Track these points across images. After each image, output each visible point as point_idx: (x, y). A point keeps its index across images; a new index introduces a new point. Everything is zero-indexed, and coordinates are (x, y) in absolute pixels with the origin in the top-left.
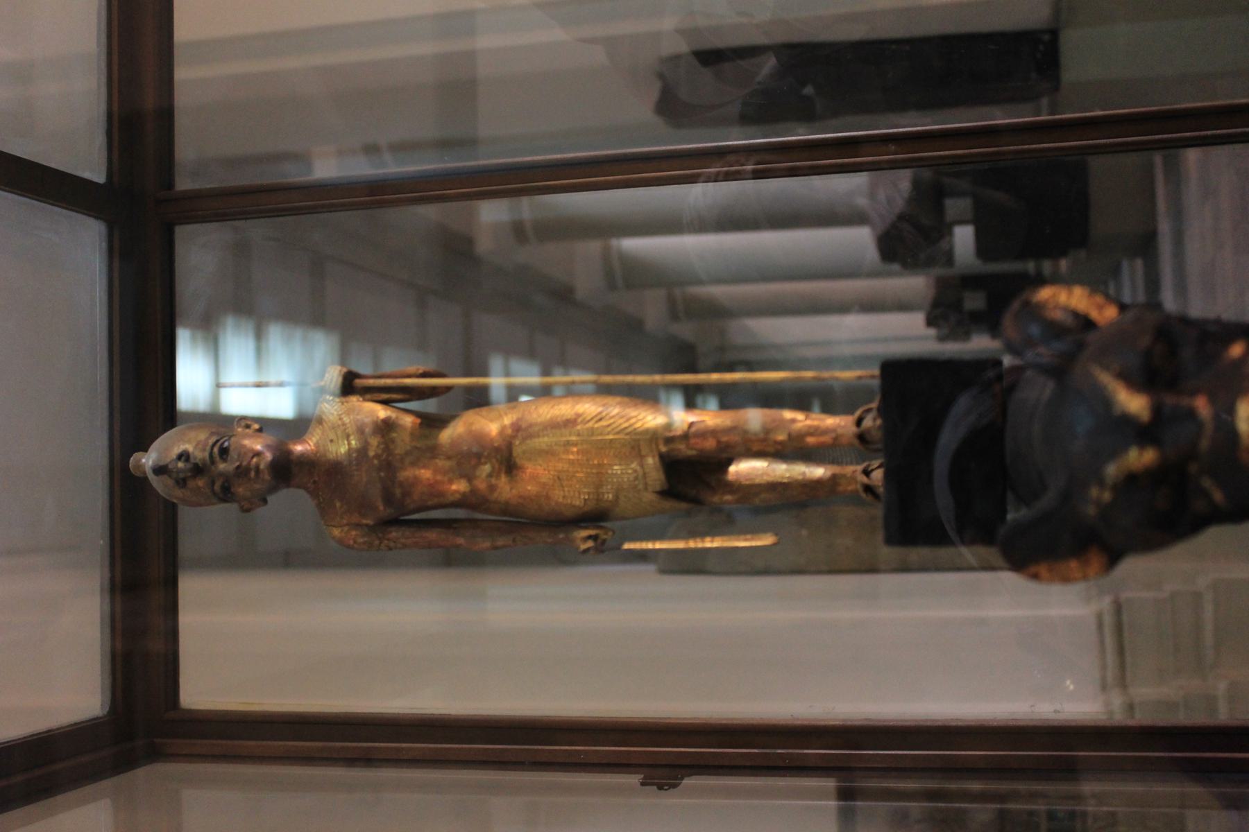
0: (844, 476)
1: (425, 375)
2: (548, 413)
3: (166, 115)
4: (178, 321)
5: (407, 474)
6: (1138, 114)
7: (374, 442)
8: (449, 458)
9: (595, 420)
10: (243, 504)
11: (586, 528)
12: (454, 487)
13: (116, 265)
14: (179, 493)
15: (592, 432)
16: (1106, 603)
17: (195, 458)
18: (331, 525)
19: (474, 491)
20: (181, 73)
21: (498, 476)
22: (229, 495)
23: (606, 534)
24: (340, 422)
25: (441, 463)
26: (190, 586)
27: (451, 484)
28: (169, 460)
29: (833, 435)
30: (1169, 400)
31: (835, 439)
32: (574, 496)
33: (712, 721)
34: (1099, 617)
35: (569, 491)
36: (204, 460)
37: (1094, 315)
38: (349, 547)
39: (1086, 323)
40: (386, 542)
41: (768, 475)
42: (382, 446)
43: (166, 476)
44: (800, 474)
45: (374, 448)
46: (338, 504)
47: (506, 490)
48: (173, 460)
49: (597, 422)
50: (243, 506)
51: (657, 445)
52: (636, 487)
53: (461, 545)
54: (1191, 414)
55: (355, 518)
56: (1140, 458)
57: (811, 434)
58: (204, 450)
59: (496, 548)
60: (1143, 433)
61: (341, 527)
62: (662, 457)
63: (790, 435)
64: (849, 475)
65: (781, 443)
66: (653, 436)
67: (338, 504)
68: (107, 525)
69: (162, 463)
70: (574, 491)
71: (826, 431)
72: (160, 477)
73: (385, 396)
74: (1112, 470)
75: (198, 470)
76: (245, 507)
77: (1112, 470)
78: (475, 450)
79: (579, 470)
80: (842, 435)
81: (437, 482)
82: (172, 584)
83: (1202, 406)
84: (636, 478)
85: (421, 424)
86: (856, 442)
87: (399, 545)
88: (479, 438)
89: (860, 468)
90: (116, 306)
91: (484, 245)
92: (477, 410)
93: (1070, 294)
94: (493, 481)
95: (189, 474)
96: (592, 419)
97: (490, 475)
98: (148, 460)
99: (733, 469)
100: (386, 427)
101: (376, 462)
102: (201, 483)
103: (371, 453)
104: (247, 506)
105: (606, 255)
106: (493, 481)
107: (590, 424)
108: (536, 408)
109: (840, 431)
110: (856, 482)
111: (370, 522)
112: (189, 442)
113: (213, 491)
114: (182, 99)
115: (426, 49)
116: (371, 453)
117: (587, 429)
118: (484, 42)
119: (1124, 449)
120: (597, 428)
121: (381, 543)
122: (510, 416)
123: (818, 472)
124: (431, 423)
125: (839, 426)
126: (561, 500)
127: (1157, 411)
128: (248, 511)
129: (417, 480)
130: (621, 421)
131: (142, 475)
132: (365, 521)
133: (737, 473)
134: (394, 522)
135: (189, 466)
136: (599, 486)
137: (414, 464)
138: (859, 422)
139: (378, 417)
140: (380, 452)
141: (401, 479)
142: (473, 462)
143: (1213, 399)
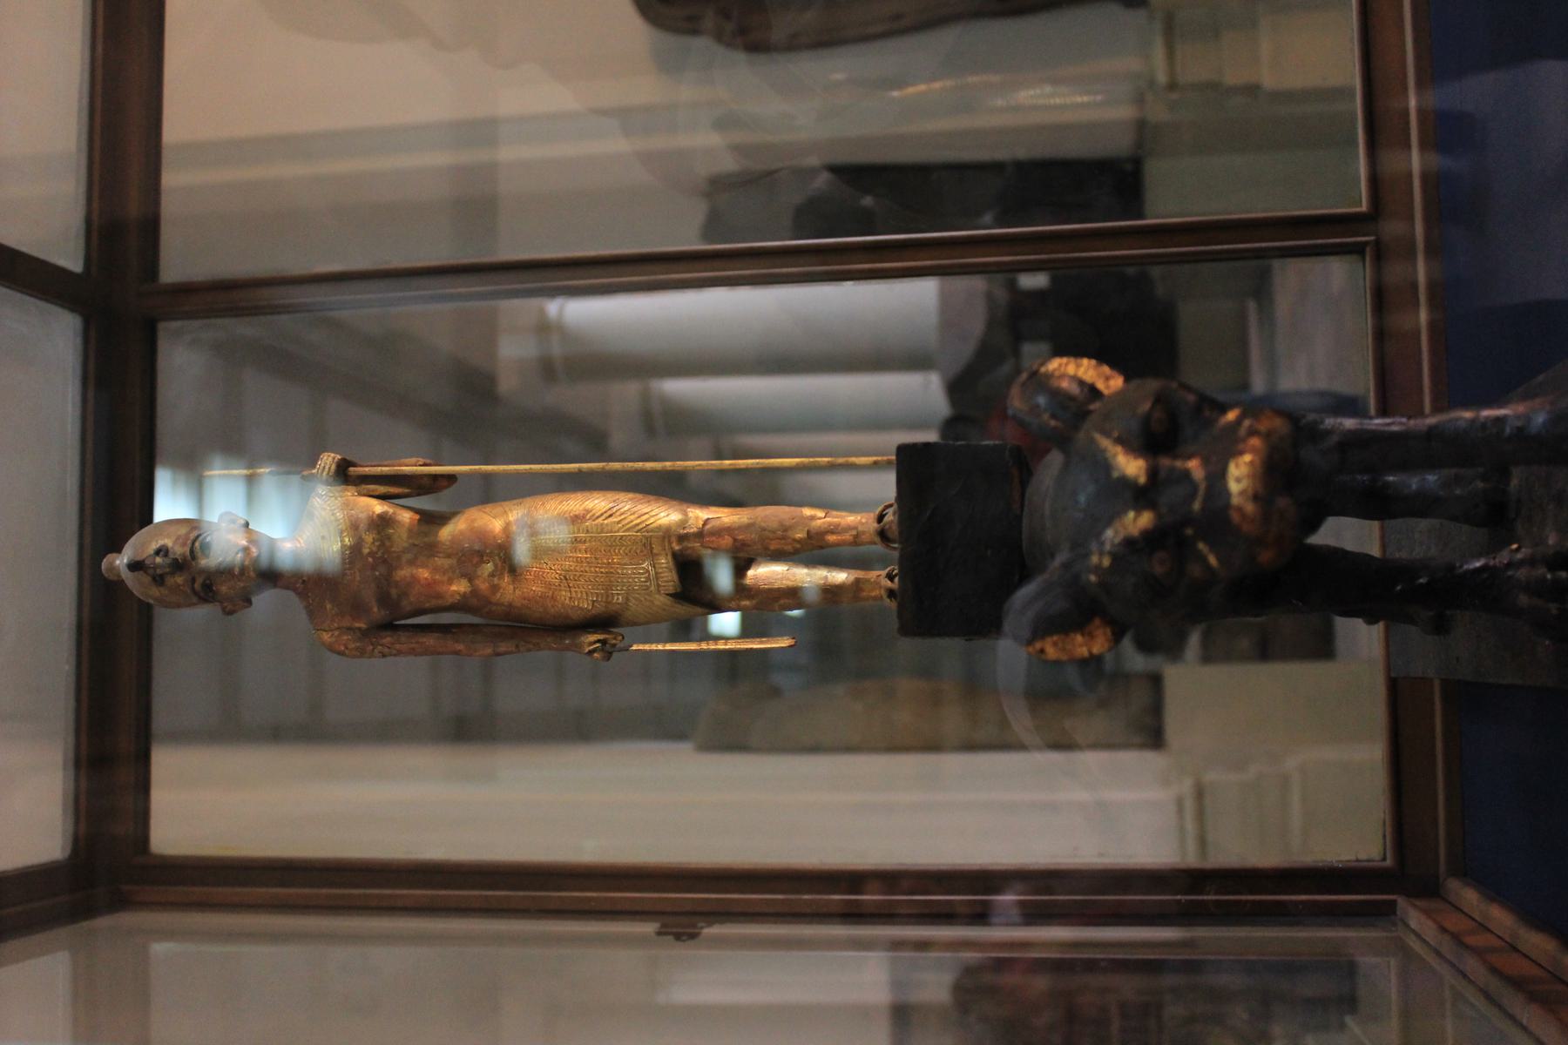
0: (868, 581)
1: (425, 465)
2: (555, 509)
3: (151, 226)
4: (158, 459)
5: (403, 573)
6: (1192, 223)
7: (369, 538)
8: (449, 556)
9: (603, 517)
10: (225, 604)
11: (595, 633)
12: (454, 588)
13: (91, 394)
14: (155, 591)
15: (602, 528)
16: (1187, 786)
17: (175, 554)
18: (321, 630)
19: (475, 592)
20: (171, 178)
21: (501, 576)
22: (210, 594)
23: (615, 639)
24: (333, 518)
25: (441, 561)
26: (165, 762)
27: (451, 585)
28: (145, 556)
29: (854, 532)
30: (1165, 462)
31: (856, 537)
32: (581, 599)
33: (735, 867)
34: (1180, 803)
35: (576, 592)
36: (184, 555)
37: (1100, 385)
38: (340, 653)
39: (1093, 392)
40: (380, 647)
41: (788, 579)
42: (377, 544)
43: (141, 572)
44: (821, 579)
45: (367, 546)
46: (329, 606)
47: (509, 592)
48: (150, 556)
49: (606, 518)
50: (226, 607)
51: (670, 543)
52: (648, 588)
53: (460, 651)
54: (1186, 474)
55: (347, 622)
56: (1137, 522)
57: (832, 532)
58: (184, 544)
59: (498, 654)
60: (1141, 496)
61: (332, 630)
62: (675, 555)
63: (808, 532)
64: (872, 580)
65: (799, 541)
66: (666, 534)
67: (329, 606)
68: (74, 652)
69: (138, 558)
70: (581, 592)
71: (849, 528)
72: (136, 573)
73: (382, 489)
74: (1111, 535)
75: (179, 566)
76: (227, 610)
77: (1111, 535)
78: (476, 548)
79: (587, 569)
80: (864, 533)
81: (435, 582)
82: (143, 759)
83: (1194, 466)
84: (648, 579)
85: (419, 520)
86: (877, 539)
87: (394, 652)
88: (482, 535)
89: (884, 573)
90: (89, 456)
91: (507, 384)
92: (480, 507)
93: (1078, 366)
94: (496, 580)
95: (168, 570)
96: (602, 515)
97: (492, 575)
98: (120, 561)
99: (750, 573)
100: (383, 522)
101: (370, 560)
102: (179, 579)
103: (366, 551)
104: (229, 607)
105: (646, 397)
106: (496, 580)
107: (600, 520)
108: (543, 504)
109: (860, 528)
110: (881, 587)
111: (363, 626)
112: (168, 536)
113: (193, 589)
114: (170, 208)
115: (442, 159)
116: (366, 551)
117: (597, 525)
118: (507, 153)
119: (1120, 514)
120: (607, 525)
121: (374, 649)
122: (515, 512)
123: (840, 577)
124: (431, 520)
125: (860, 522)
126: (567, 601)
127: (1153, 473)
128: (230, 613)
129: (415, 579)
130: (632, 517)
131: (116, 578)
132: (357, 625)
133: (756, 577)
134: (389, 626)
135: (168, 561)
136: (609, 587)
137: (412, 563)
138: (880, 518)
139: (374, 512)
140: (374, 549)
141: (398, 579)
142: (475, 560)
143: (1206, 462)
